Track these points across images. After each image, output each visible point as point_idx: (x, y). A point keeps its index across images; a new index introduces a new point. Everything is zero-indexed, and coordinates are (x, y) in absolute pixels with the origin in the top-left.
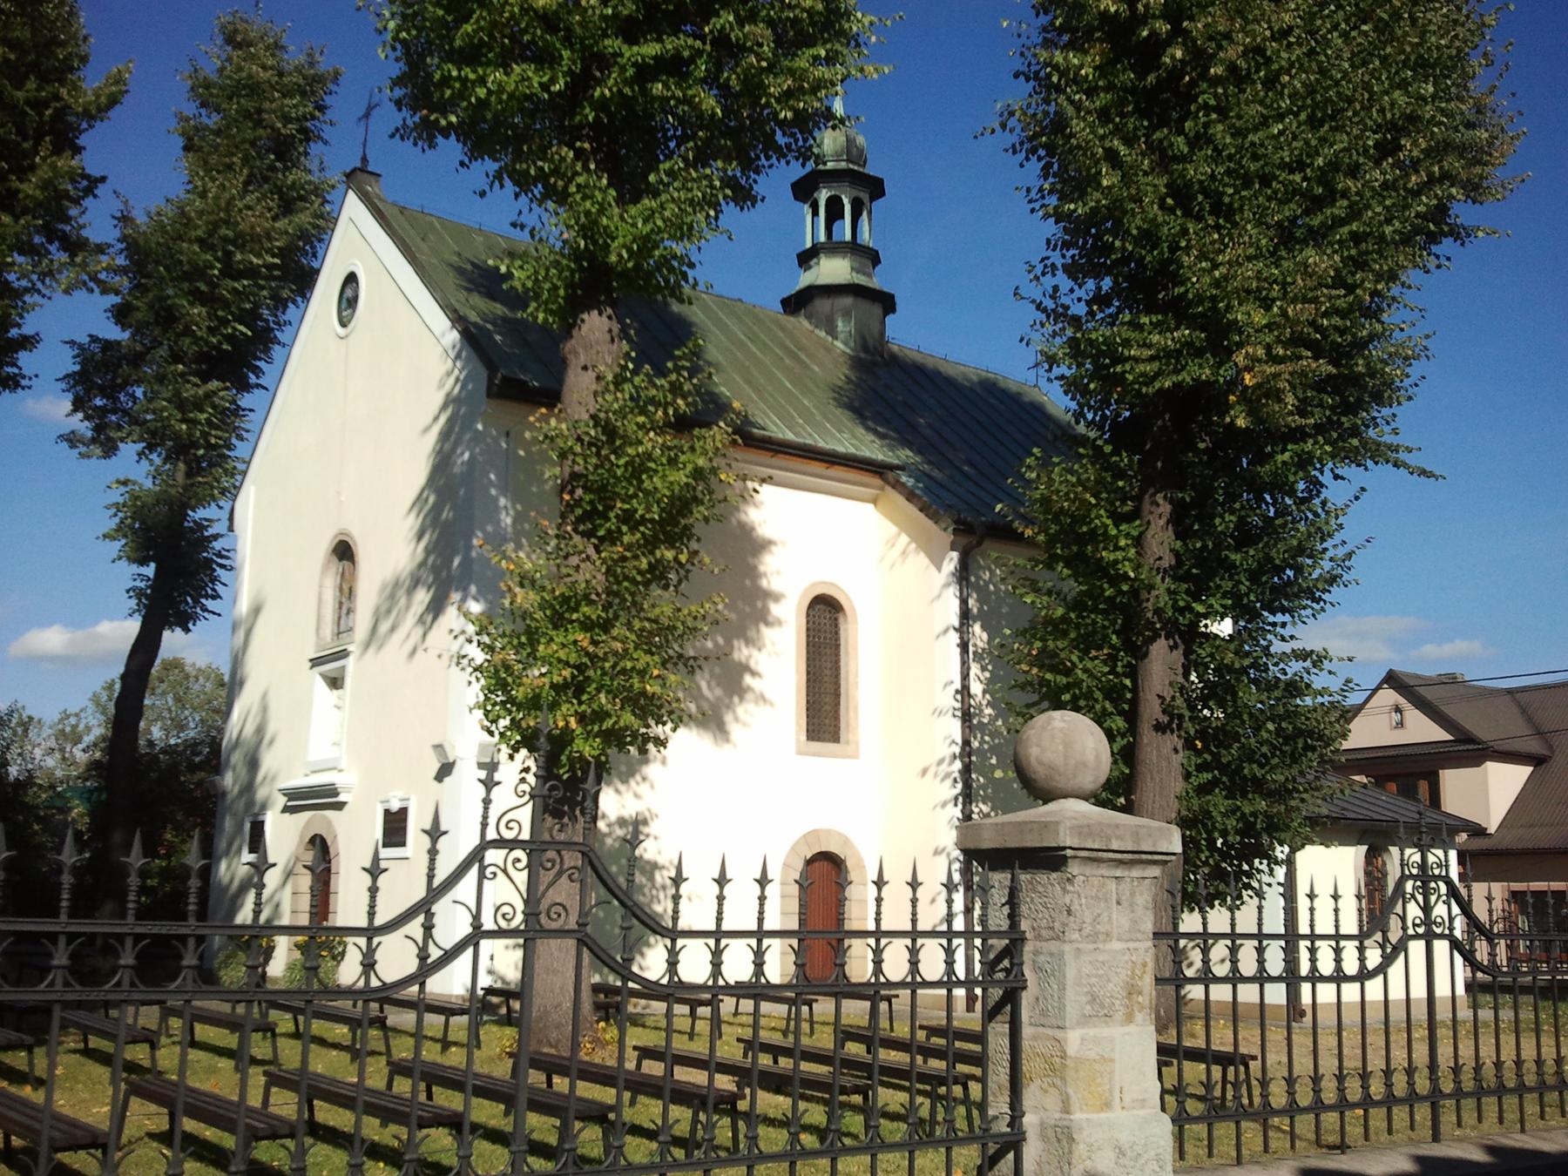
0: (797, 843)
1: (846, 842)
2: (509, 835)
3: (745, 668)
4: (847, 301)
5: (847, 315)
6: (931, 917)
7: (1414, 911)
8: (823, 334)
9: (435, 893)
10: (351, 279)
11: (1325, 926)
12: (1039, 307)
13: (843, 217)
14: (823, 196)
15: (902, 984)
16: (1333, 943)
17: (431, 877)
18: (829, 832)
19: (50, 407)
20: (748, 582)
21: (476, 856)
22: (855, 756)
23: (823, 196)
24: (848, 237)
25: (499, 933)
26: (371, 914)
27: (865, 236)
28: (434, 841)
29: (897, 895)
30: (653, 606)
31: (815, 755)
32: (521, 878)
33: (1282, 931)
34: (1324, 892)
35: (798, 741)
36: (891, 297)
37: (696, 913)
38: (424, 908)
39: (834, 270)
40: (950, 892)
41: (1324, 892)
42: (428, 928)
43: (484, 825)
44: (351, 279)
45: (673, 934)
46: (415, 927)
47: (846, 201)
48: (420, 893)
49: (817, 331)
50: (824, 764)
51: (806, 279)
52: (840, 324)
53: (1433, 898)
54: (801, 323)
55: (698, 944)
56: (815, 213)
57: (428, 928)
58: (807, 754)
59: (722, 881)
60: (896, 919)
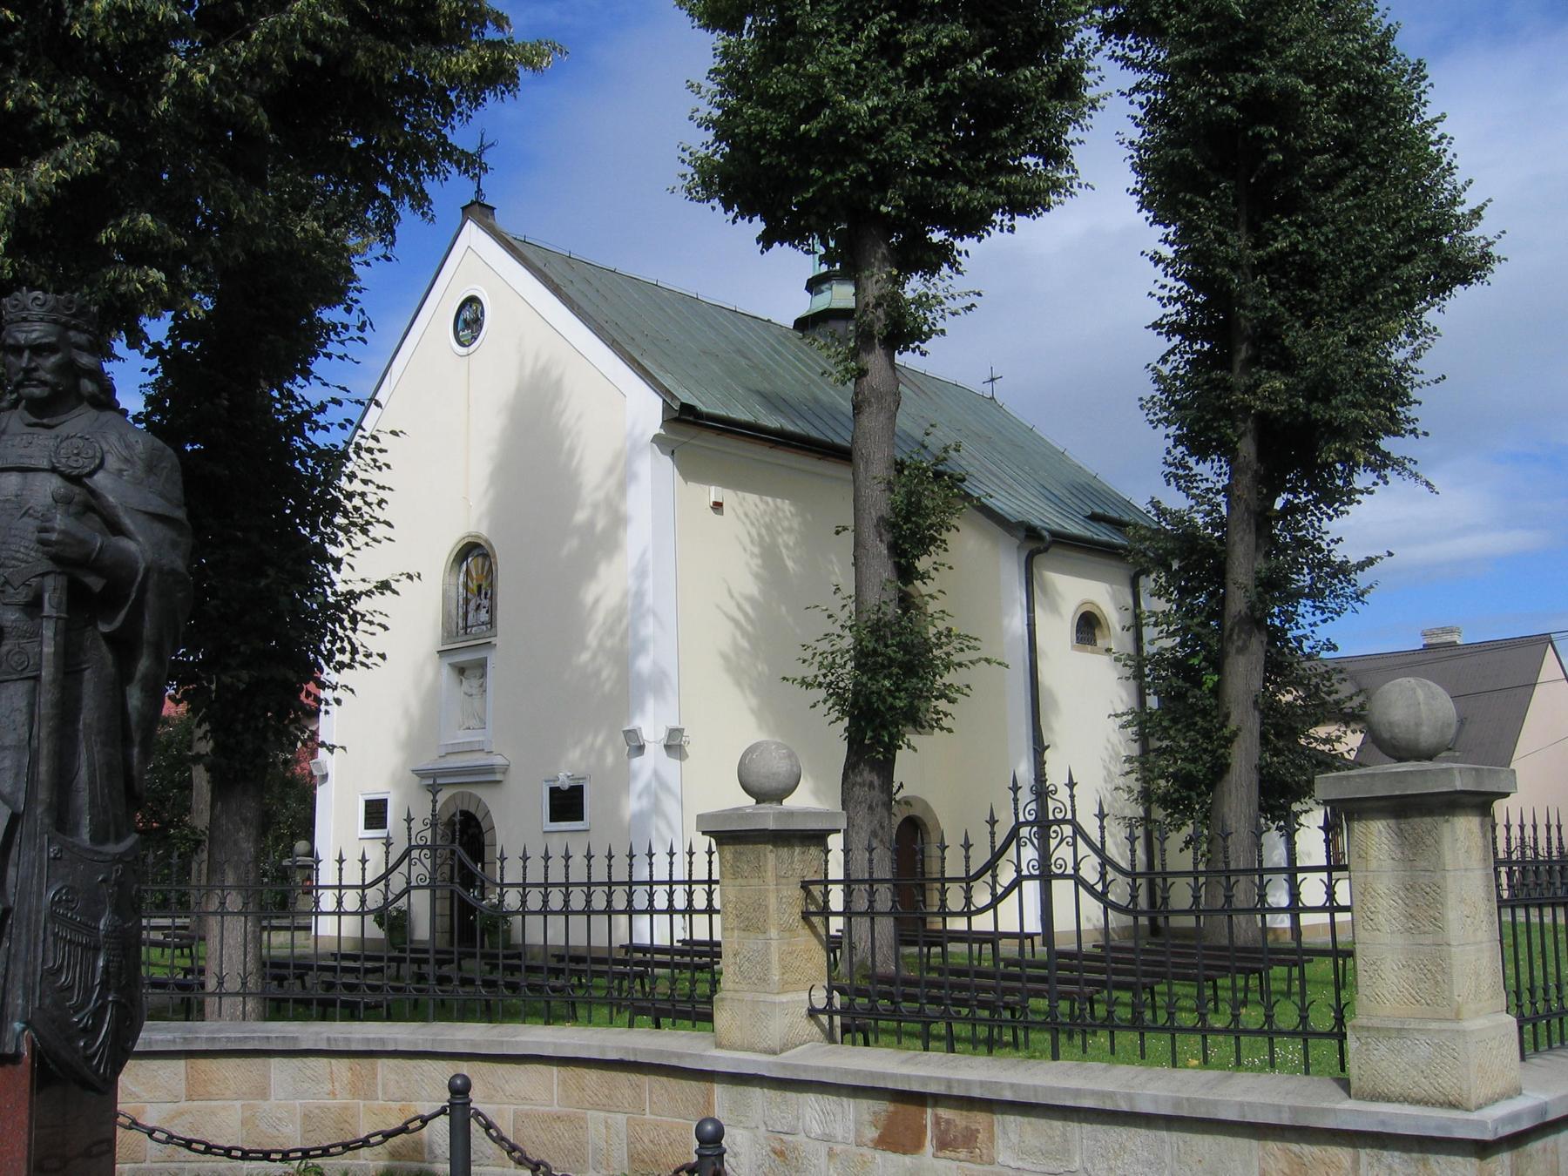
2: (1060, 816)
6: (700, 873)
7: (1029, 854)
9: (997, 855)
11: (661, 873)
12: (805, 683)
15: (517, 912)
16: (1191, 880)
17: (993, 847)
20: (1152, 702)
21: (407, 853)
25: (419, 887)
26: (967, 872)
28: (992, 826)
29: (661, 860)
32: (428, 863)
33: (1324, 863)
34: (1515, 823)
37: (513, 874)
38: (385, 877)
40: (1132, 844)
41: (1515, 823)
42: (387, 886)
43: (1016, 815)
45: (502, 885)
46: (381, 885)
48: (383, 871)
53: (1053, 843)
55: (330, 892)
57: (387, 886)
59: (610, 857)
60: (557, 875)
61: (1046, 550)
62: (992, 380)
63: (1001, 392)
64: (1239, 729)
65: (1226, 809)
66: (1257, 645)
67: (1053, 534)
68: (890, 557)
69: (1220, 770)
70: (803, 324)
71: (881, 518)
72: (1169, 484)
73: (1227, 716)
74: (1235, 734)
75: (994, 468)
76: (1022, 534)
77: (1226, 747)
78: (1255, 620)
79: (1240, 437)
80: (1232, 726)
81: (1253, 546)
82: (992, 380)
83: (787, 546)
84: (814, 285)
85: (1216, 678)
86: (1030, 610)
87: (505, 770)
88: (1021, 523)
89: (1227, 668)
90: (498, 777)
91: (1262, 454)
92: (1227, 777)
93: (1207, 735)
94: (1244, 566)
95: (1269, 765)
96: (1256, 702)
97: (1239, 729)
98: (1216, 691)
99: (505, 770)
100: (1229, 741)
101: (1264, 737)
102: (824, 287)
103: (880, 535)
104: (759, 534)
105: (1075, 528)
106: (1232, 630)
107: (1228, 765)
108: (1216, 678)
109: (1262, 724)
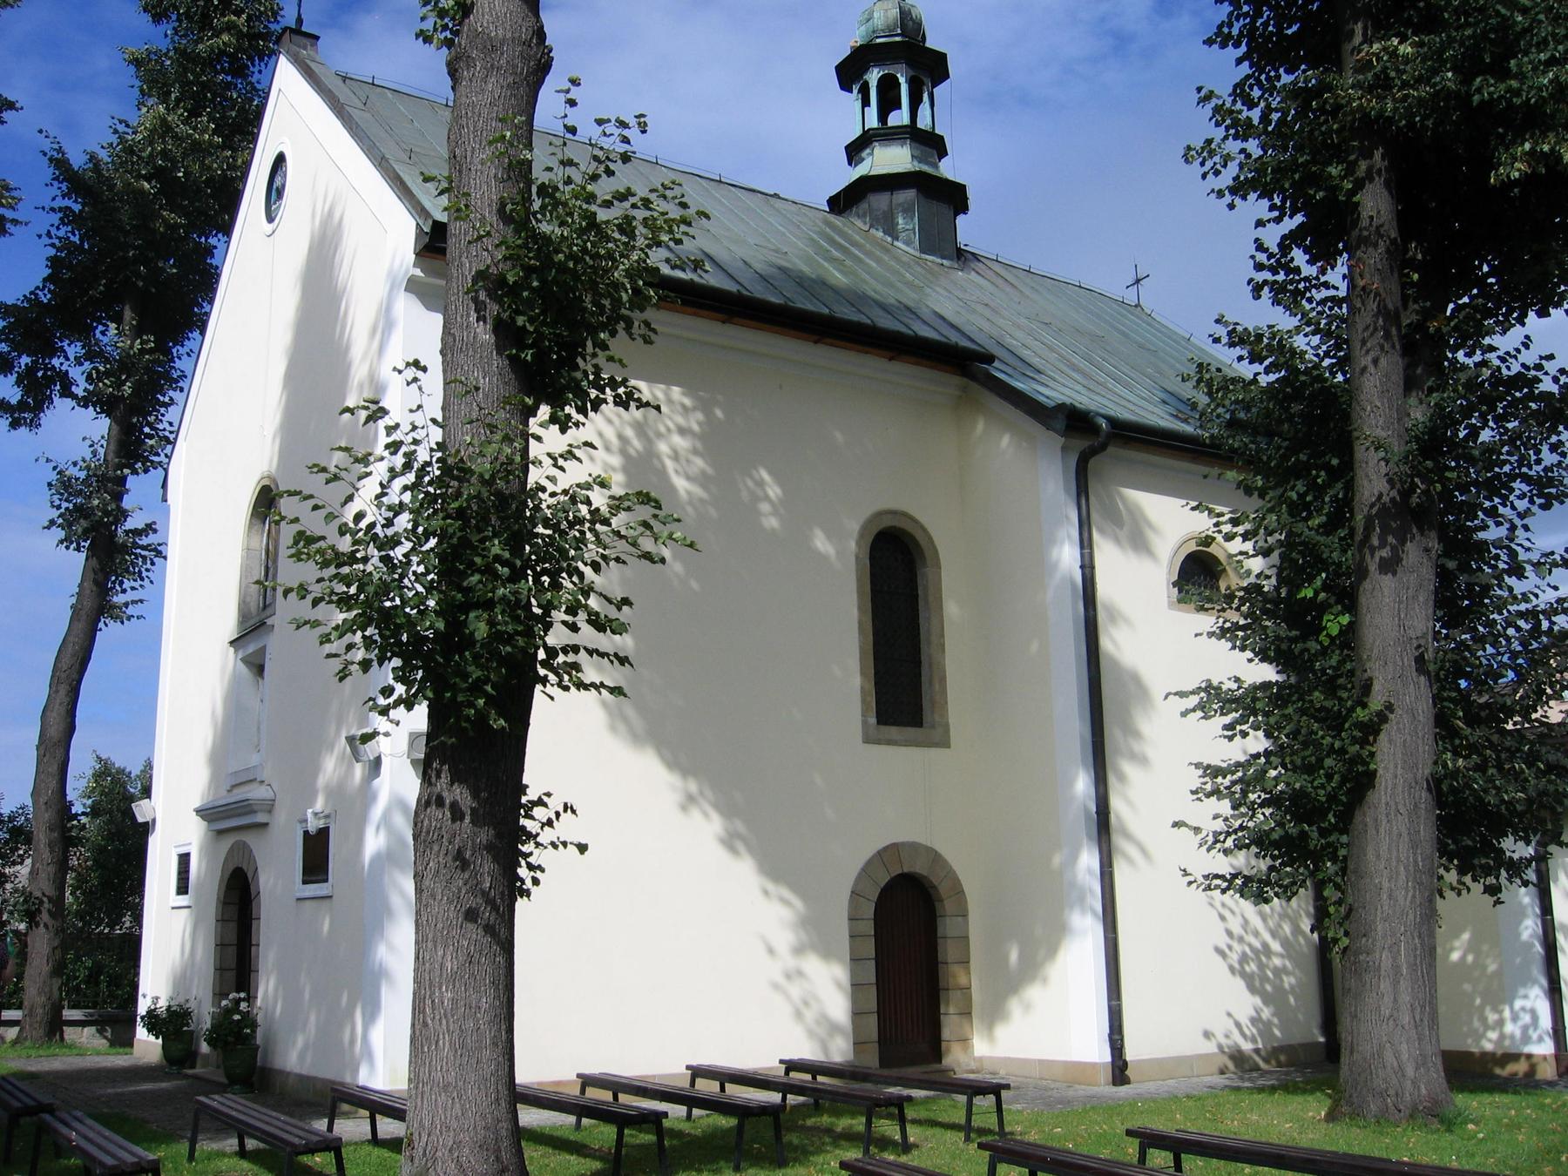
0: (869, 863)
1: (936, 858)
3: (1254, 888)
4: (909, 195)
5: (907, 211)
8: (880, 234)
10: (280, 160)
13: (899, 107)
14: (873, 76)
18: (914, 847)
19: (12, 378)
22: (944, 743)
23: (873, 76)
24: (906, 120)
27: (924, 122)
30: (1514, 1126)
31: (890, 742)
35: (865, 723)
36: (961, 189)
39: (892, 159)
44: (280, 160)
47: (902, 80)
49: (873, 231)
50: (900, 761)
51: (862, 170)
52: (900, 221)
54: (855, 225)
56: (866, 103)
58: (878, 742)
61: (1103, 447)
62: (1138, 281)
63: (1149, 297)
64: (1390, 707)
65: (1371, 856)
66: (1420, 557)
67: (1114, 422)
68: (500, 349)
69: (1361, 782)
70: (843, 202)
71: (481, 275)
72: (1257, 297)
73: (1367, 687)
74: (1382, 717)
75: (1083, 365)
76: (1061, 423)
77: (1364, 742)
78: (1406, 514)
79: (1359, 185)
80: (1376, 703)
81: (1397, 378)
82: (1138, 281)
83: (676, 456)
84: (855, 151)
85: (1345, 619)
86: (1086, 544)
87: (270, 806)
88: (1061, 407)
89: (1363, 600)
90: (261, 818)
91: (1409, 219)
92: (1372, 797)
93: (1335, 722)
94: (1384, 415)
95: (1455, 773)
96: (1420, 660)
97: (1390, 707)
98: (1349, 639)
99: (270, 806)
100: (1371, 730)
101: (1442, 722)
102: (864, 154)
103: (480, 307)
104: (621, 437)
105: (1159, 417)
106: (1368, 529)
107: (1371, 776)
108: (1345, 619)
109: (1437, 699)
